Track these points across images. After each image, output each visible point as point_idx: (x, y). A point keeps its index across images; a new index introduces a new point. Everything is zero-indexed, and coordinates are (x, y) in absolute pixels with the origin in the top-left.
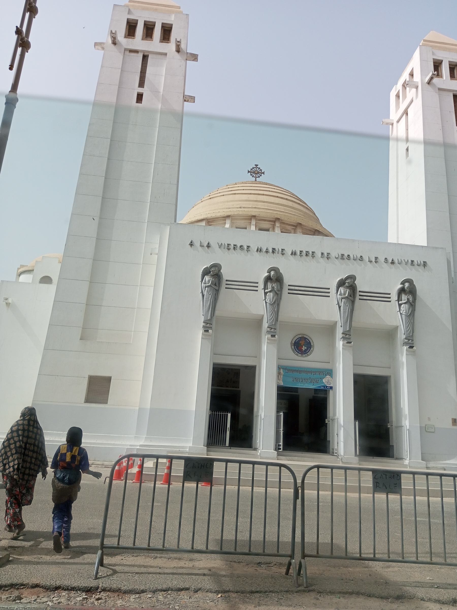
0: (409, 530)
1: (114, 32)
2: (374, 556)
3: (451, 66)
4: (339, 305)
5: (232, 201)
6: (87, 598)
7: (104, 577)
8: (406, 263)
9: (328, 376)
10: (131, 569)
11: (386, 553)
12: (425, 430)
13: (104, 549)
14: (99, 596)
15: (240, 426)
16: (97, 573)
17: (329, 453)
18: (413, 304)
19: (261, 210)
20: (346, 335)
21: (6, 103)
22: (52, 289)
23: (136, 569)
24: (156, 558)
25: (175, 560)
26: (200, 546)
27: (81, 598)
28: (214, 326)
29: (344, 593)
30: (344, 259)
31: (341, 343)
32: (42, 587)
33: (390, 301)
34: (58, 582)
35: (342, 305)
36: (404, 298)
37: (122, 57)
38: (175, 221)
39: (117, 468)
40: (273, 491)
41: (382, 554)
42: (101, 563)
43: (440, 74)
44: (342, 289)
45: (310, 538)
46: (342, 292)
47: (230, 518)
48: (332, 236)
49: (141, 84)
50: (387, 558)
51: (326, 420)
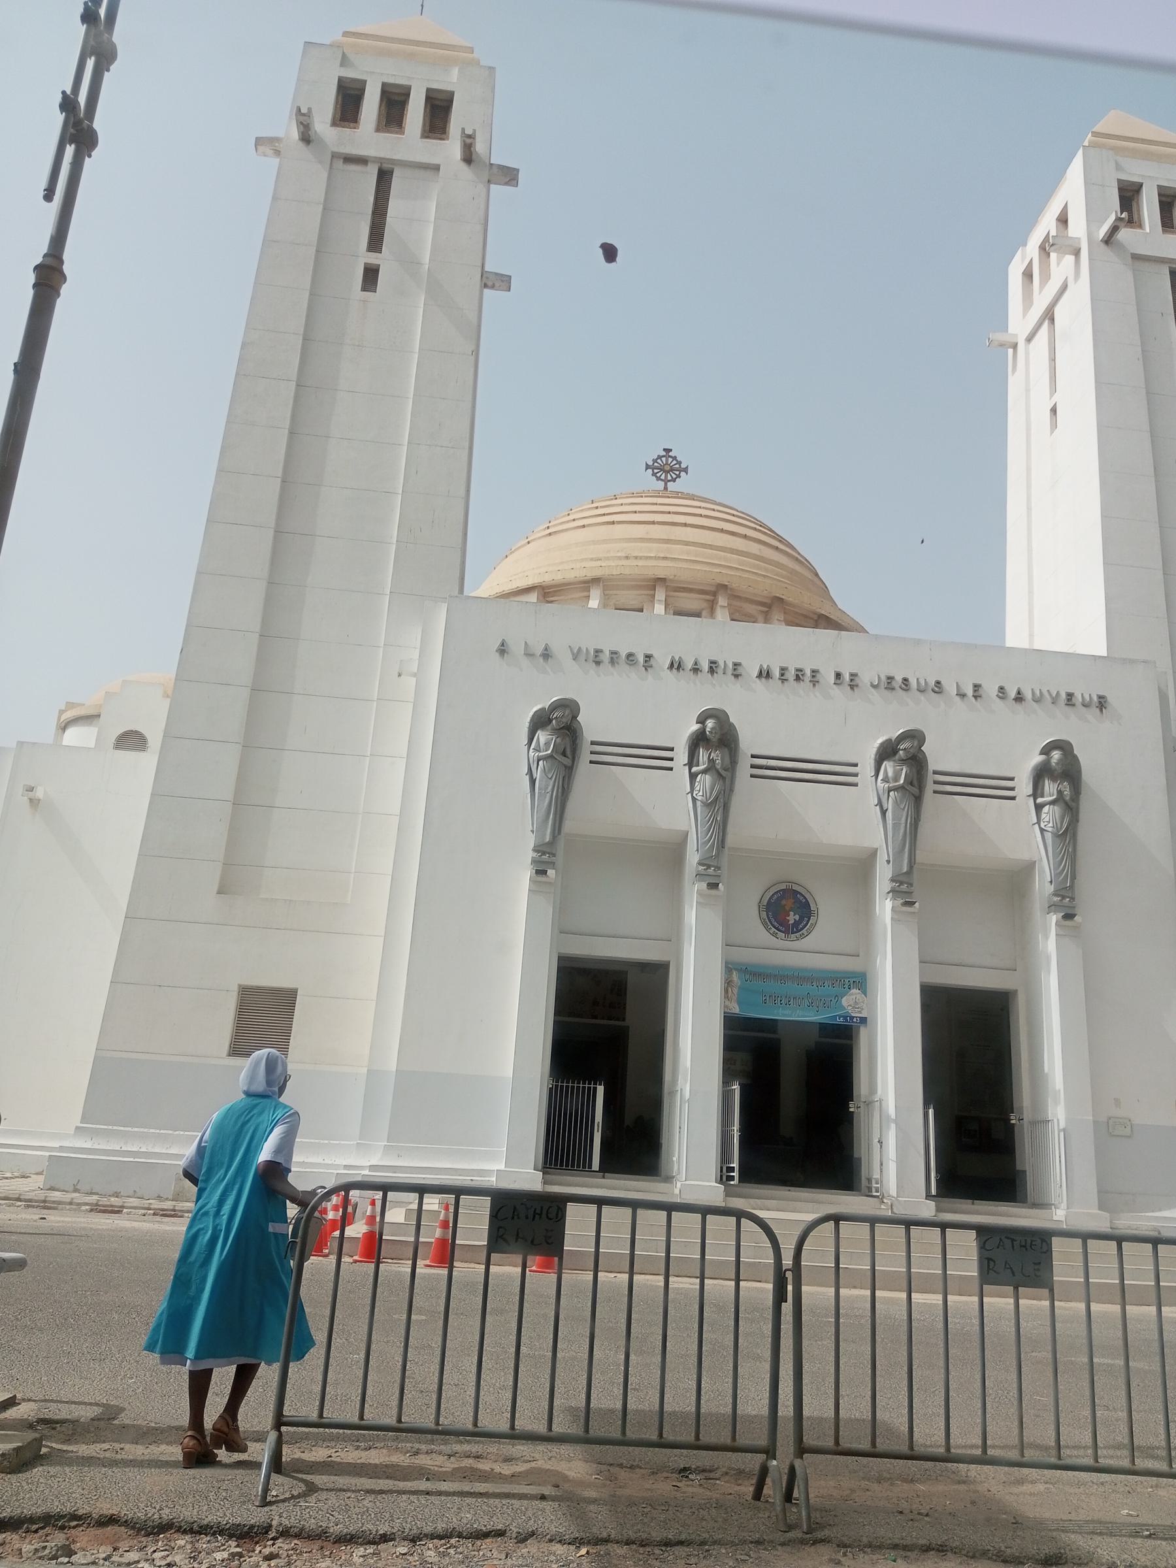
0: (1074, 1389)
1: (304, 110)
2: (985, 1451)
3: (1163, 199)
4: (881, 807)
5: (605, 541)
6: (240, 1555)
7: (284, 1501)
11: (1013, 1447)
12: (1110, 1132)
13: (283, 1429)
14: (272, 1549)
15: (629, 1120)
16: (266, 1490)
17: (859, 1190)
18: (1073, 804)
20: (901, 883)
21: (35, 286)
22: (146, 763)
26: (530, 1419)
27: (225, 1555)
28: (560, 859)
29: (906, 1548)
30: (893, 689)
31: (889, 904)
33: (1013, 798)
34: (167, 1511)
35: (890, 806)
36: (1050, 789)
37: (325, 175)
40: (720, 1288)
42: (277, 1465)
44: (889, 767)
45: (817, 1406)
46: (890, 774)
47: (609, 1354)
48: (862, 630)
49: (376, 241)
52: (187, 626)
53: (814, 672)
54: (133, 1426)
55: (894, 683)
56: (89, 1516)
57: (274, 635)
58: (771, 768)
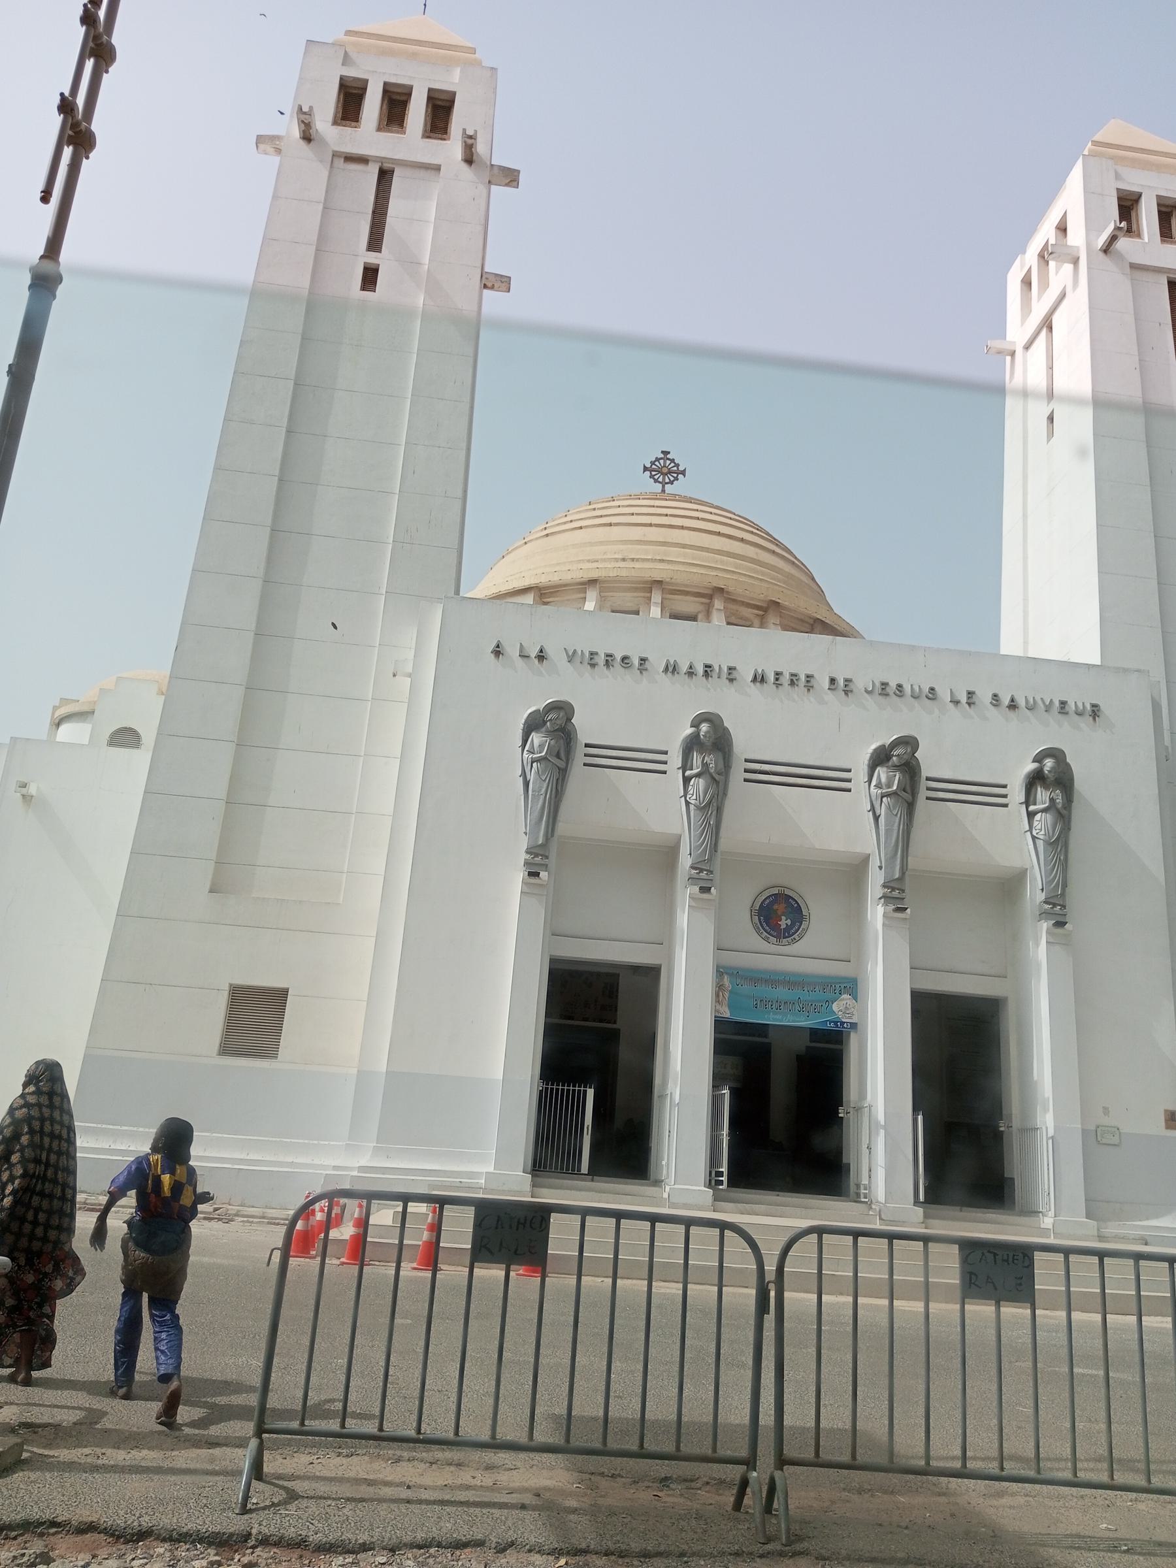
0: (1054, 1398)
1: (305, 109)
2: (964, 1465)
3: (1163, 209)
4: (874, 813)
5: (601, 543)
7: (264, 1508)
8: (1048, 708)
9: (845, 996)
10: (334, 1489)
12: (1097, 1140)
13: (265, 1436)
14: (251, 1558)
16: (246, 1497)
18: (1064, 812)
19: (676, 567)
20: (893, 889)
21: (30, 287)
22: (139, 761)
23: (347, 1491)
24: (398, 1460)
25: (447, 1468)
26: (512, 1429)
28: (552, 861)
30: (887, 695)
32: (105, 1531)
33: (1006, 806)
34: (147, 1518)
35: (882, 811)
36: (1043, 796)
37: (326, 173)
38: (457, 592)
39: (299, 1225)
41: (983, 1459)
42: (257, 1471)
43: (1134, 227)
44: (882, 773)
45: (798, 1415)
46: (883, 780)
47: (591, 1359)
49: (375, 243)
50: (997, 1471)
51: (841, 1110)
52: (183, 623)
53: (809, 677)
54: (115, 1430)
55: (888, 690)
56: (68, 1523)
57: (268, 634)
58: (764, 773)
